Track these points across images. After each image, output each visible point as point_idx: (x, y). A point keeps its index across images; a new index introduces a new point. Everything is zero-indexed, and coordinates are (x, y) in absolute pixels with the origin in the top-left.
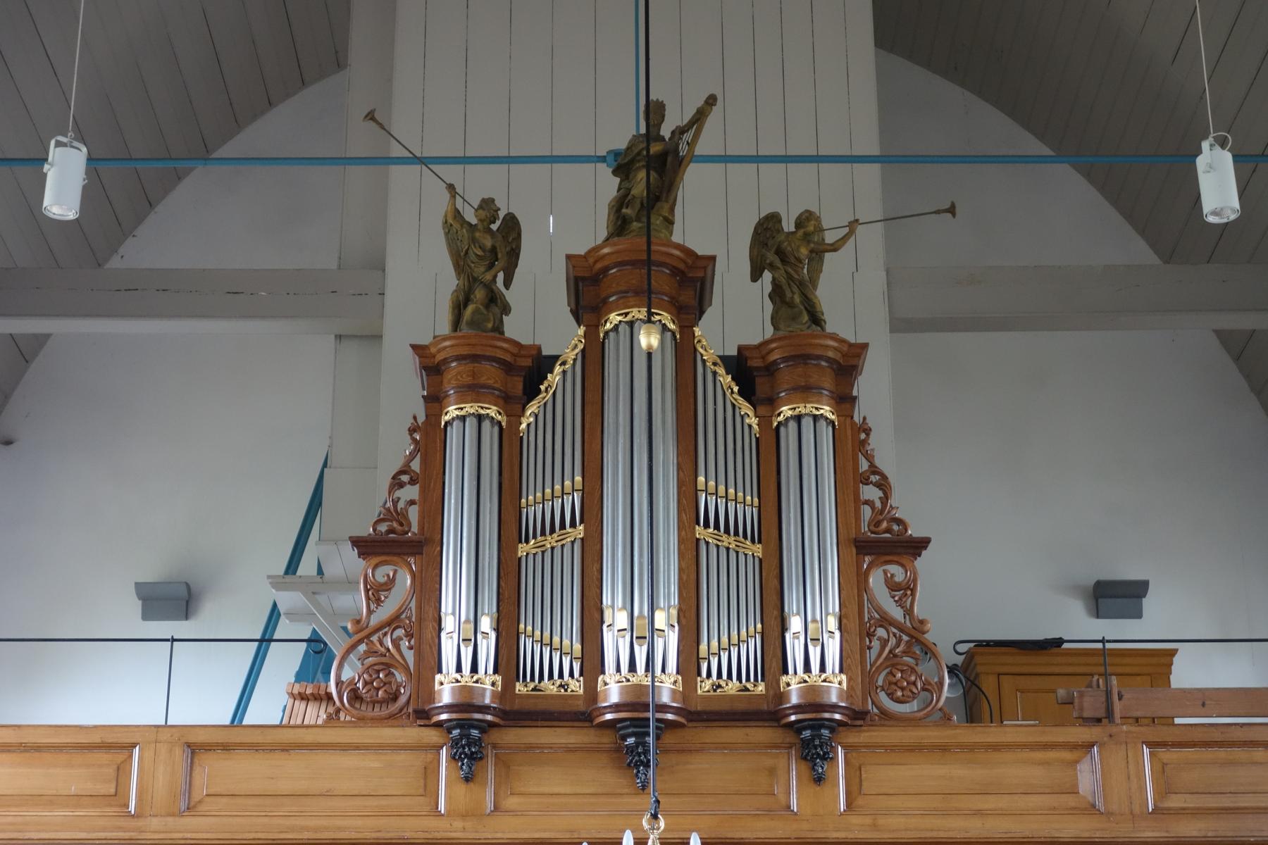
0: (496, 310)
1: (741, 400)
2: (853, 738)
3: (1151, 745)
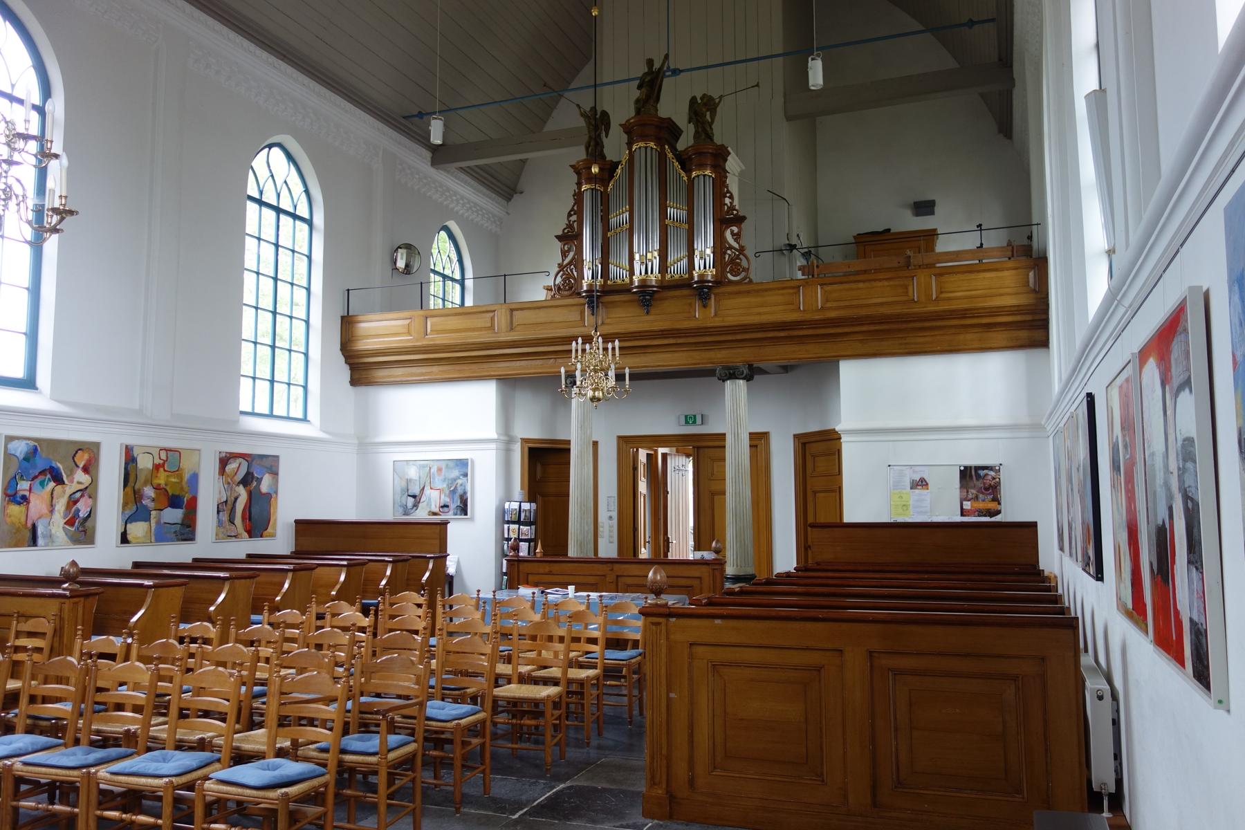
1: (682, 171)
2: (716, 291)
3: (821, 285)
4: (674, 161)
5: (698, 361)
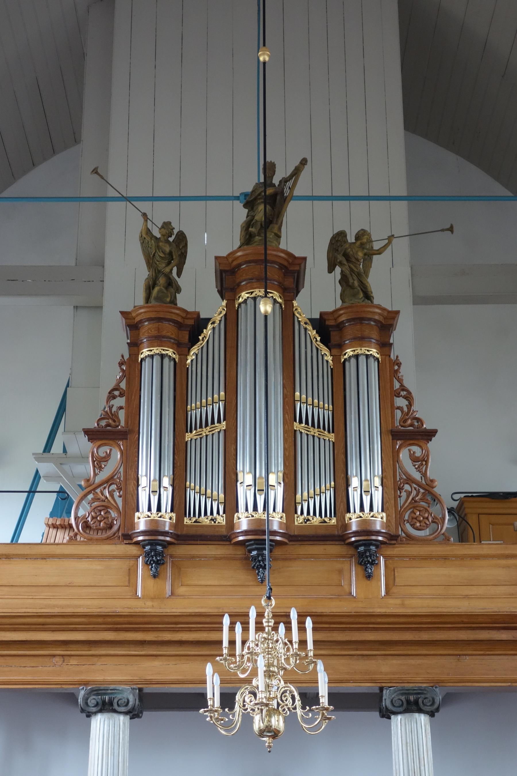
0: (172, 290)
1: (322, 345)
2: (390, 551)
4: (309, 327)
5: (347, 677)
